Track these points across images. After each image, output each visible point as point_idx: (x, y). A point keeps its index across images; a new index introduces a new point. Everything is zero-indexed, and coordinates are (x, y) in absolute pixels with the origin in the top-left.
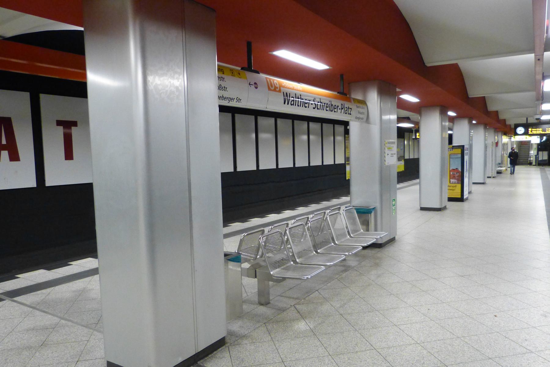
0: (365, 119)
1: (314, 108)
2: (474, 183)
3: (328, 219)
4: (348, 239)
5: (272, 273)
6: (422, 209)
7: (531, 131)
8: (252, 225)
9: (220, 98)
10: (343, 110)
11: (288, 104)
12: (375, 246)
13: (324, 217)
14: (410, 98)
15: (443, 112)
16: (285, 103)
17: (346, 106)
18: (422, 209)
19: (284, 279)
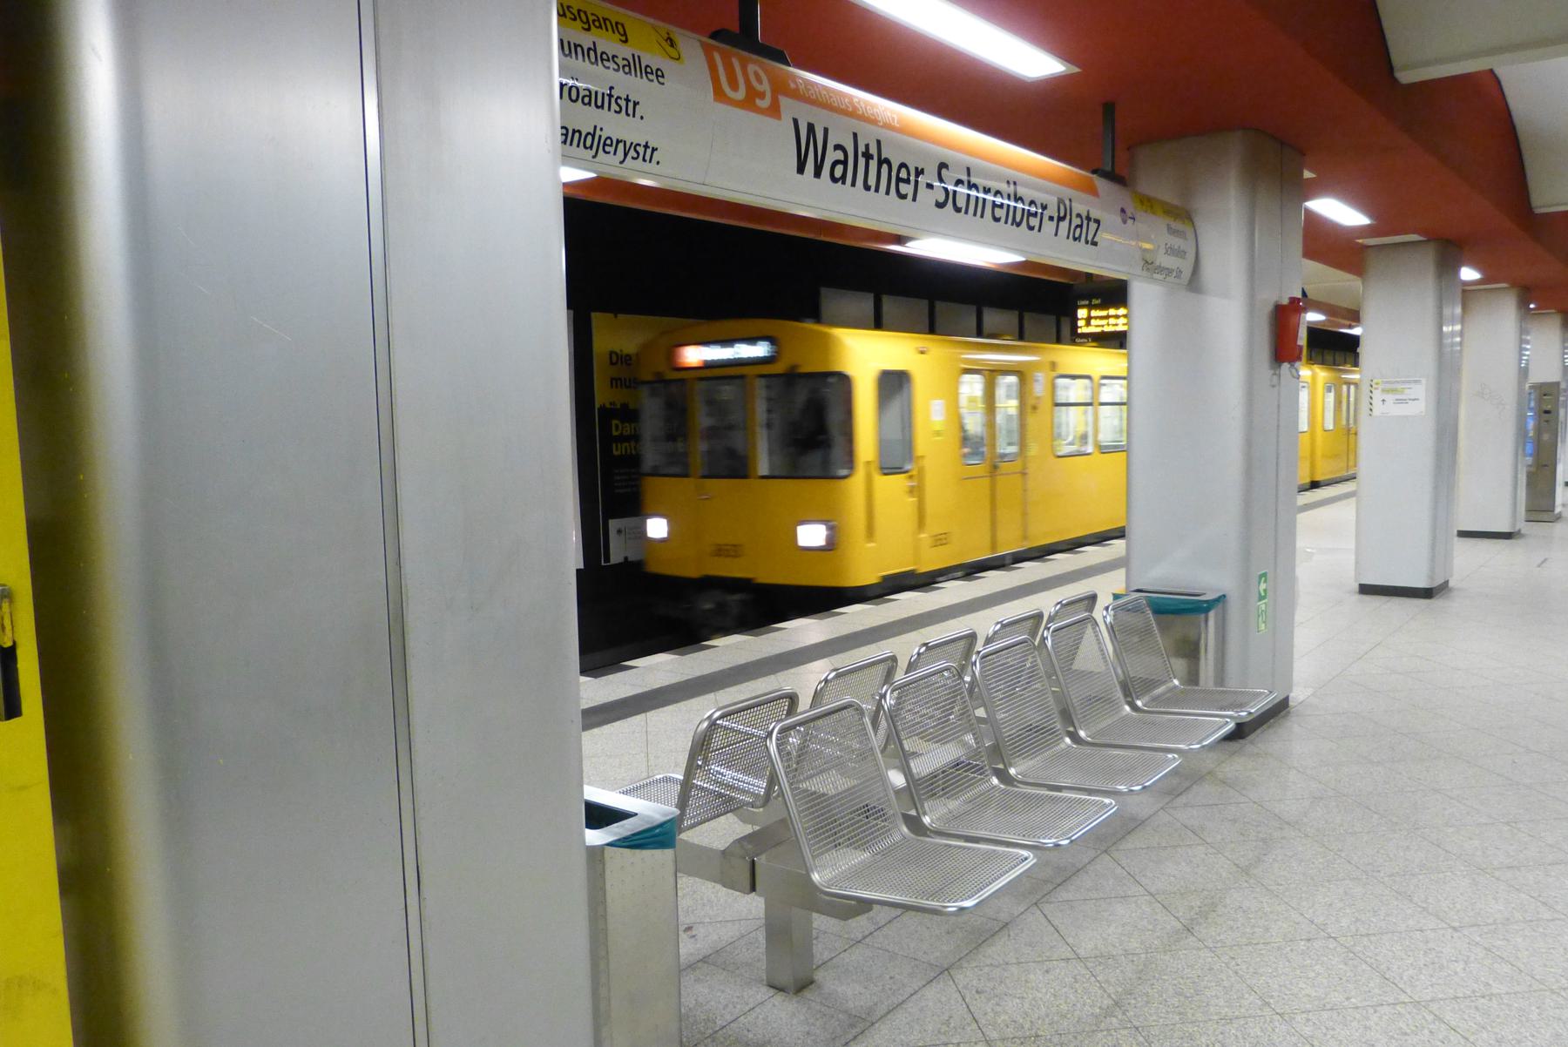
0: (1187, 273)
1: (940, 205)
2: (1464, 534)
3: (1049, 643)
4: (1067, 753)
5: (816, 877)
6: (1366, 590)
7: (1088, 320)
8: (695, 703)
9: (569, 136)
10: (1064, 225)
11: (817, 174)
12: (1240, 732)
13: (1033, 633)
14: (1338, 211)
15: (1447, 266)
16: (801, 170)
17: (1078, 208)
18: (1366, 590)
19: (865, 905)
